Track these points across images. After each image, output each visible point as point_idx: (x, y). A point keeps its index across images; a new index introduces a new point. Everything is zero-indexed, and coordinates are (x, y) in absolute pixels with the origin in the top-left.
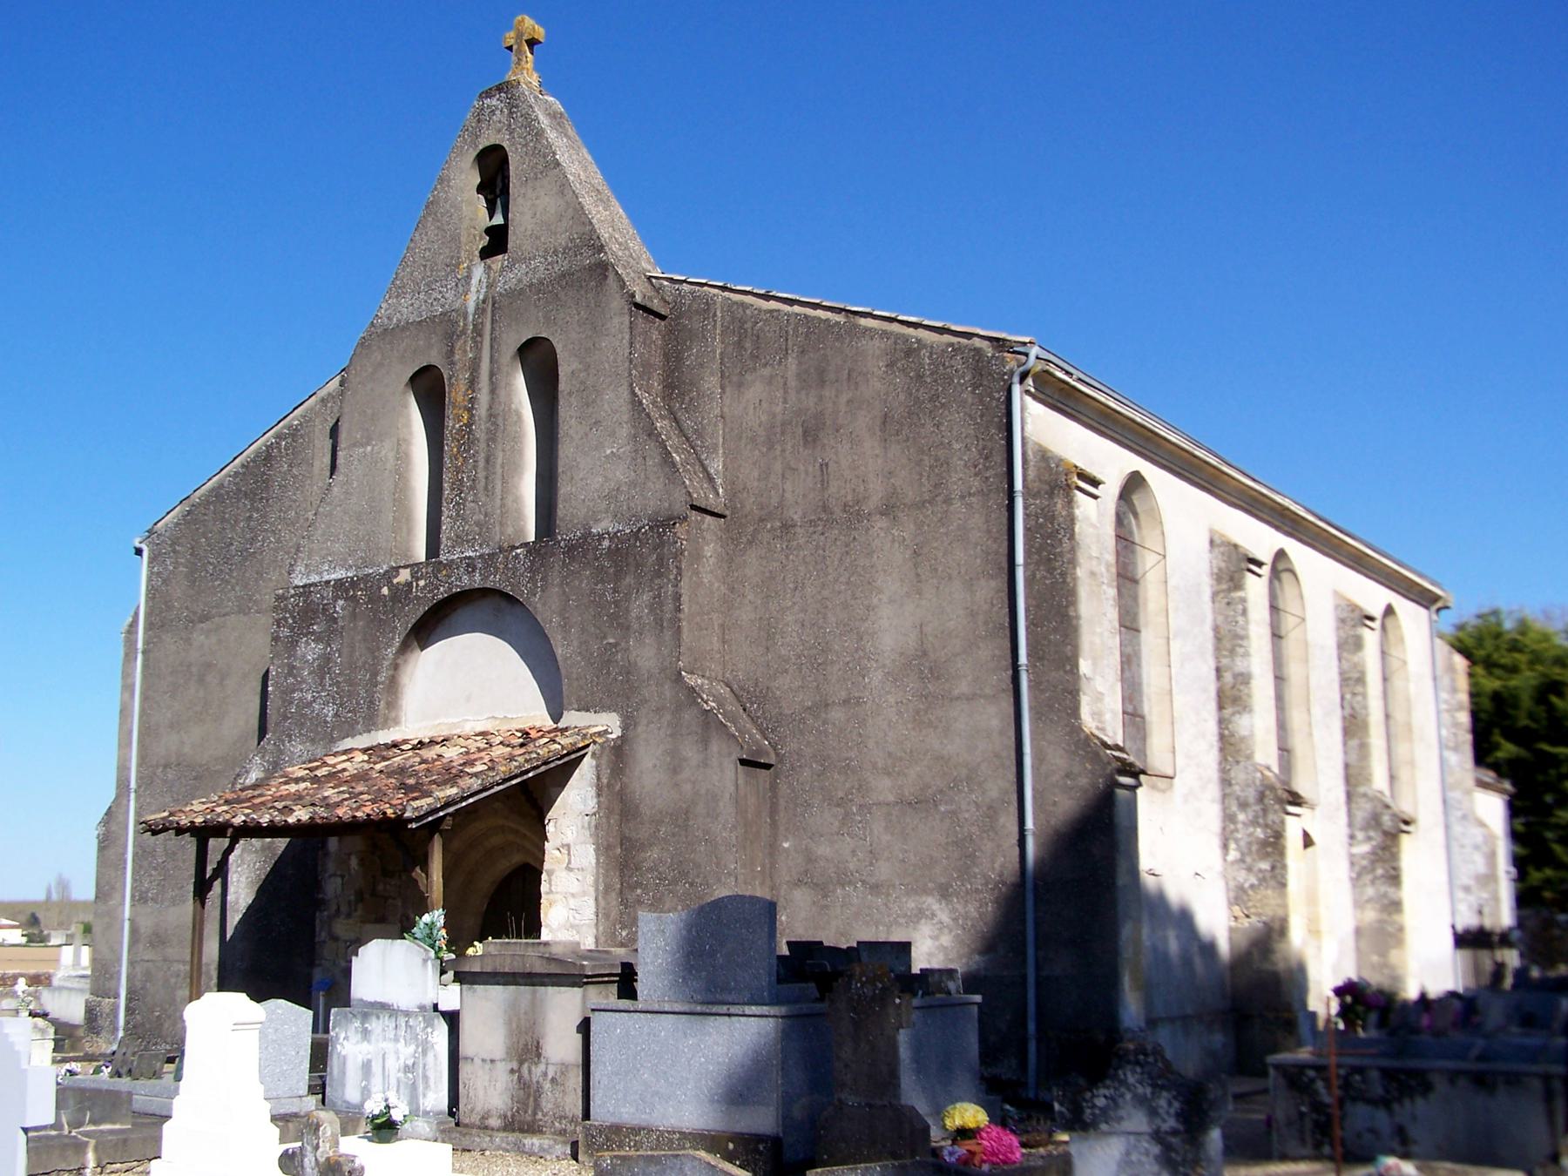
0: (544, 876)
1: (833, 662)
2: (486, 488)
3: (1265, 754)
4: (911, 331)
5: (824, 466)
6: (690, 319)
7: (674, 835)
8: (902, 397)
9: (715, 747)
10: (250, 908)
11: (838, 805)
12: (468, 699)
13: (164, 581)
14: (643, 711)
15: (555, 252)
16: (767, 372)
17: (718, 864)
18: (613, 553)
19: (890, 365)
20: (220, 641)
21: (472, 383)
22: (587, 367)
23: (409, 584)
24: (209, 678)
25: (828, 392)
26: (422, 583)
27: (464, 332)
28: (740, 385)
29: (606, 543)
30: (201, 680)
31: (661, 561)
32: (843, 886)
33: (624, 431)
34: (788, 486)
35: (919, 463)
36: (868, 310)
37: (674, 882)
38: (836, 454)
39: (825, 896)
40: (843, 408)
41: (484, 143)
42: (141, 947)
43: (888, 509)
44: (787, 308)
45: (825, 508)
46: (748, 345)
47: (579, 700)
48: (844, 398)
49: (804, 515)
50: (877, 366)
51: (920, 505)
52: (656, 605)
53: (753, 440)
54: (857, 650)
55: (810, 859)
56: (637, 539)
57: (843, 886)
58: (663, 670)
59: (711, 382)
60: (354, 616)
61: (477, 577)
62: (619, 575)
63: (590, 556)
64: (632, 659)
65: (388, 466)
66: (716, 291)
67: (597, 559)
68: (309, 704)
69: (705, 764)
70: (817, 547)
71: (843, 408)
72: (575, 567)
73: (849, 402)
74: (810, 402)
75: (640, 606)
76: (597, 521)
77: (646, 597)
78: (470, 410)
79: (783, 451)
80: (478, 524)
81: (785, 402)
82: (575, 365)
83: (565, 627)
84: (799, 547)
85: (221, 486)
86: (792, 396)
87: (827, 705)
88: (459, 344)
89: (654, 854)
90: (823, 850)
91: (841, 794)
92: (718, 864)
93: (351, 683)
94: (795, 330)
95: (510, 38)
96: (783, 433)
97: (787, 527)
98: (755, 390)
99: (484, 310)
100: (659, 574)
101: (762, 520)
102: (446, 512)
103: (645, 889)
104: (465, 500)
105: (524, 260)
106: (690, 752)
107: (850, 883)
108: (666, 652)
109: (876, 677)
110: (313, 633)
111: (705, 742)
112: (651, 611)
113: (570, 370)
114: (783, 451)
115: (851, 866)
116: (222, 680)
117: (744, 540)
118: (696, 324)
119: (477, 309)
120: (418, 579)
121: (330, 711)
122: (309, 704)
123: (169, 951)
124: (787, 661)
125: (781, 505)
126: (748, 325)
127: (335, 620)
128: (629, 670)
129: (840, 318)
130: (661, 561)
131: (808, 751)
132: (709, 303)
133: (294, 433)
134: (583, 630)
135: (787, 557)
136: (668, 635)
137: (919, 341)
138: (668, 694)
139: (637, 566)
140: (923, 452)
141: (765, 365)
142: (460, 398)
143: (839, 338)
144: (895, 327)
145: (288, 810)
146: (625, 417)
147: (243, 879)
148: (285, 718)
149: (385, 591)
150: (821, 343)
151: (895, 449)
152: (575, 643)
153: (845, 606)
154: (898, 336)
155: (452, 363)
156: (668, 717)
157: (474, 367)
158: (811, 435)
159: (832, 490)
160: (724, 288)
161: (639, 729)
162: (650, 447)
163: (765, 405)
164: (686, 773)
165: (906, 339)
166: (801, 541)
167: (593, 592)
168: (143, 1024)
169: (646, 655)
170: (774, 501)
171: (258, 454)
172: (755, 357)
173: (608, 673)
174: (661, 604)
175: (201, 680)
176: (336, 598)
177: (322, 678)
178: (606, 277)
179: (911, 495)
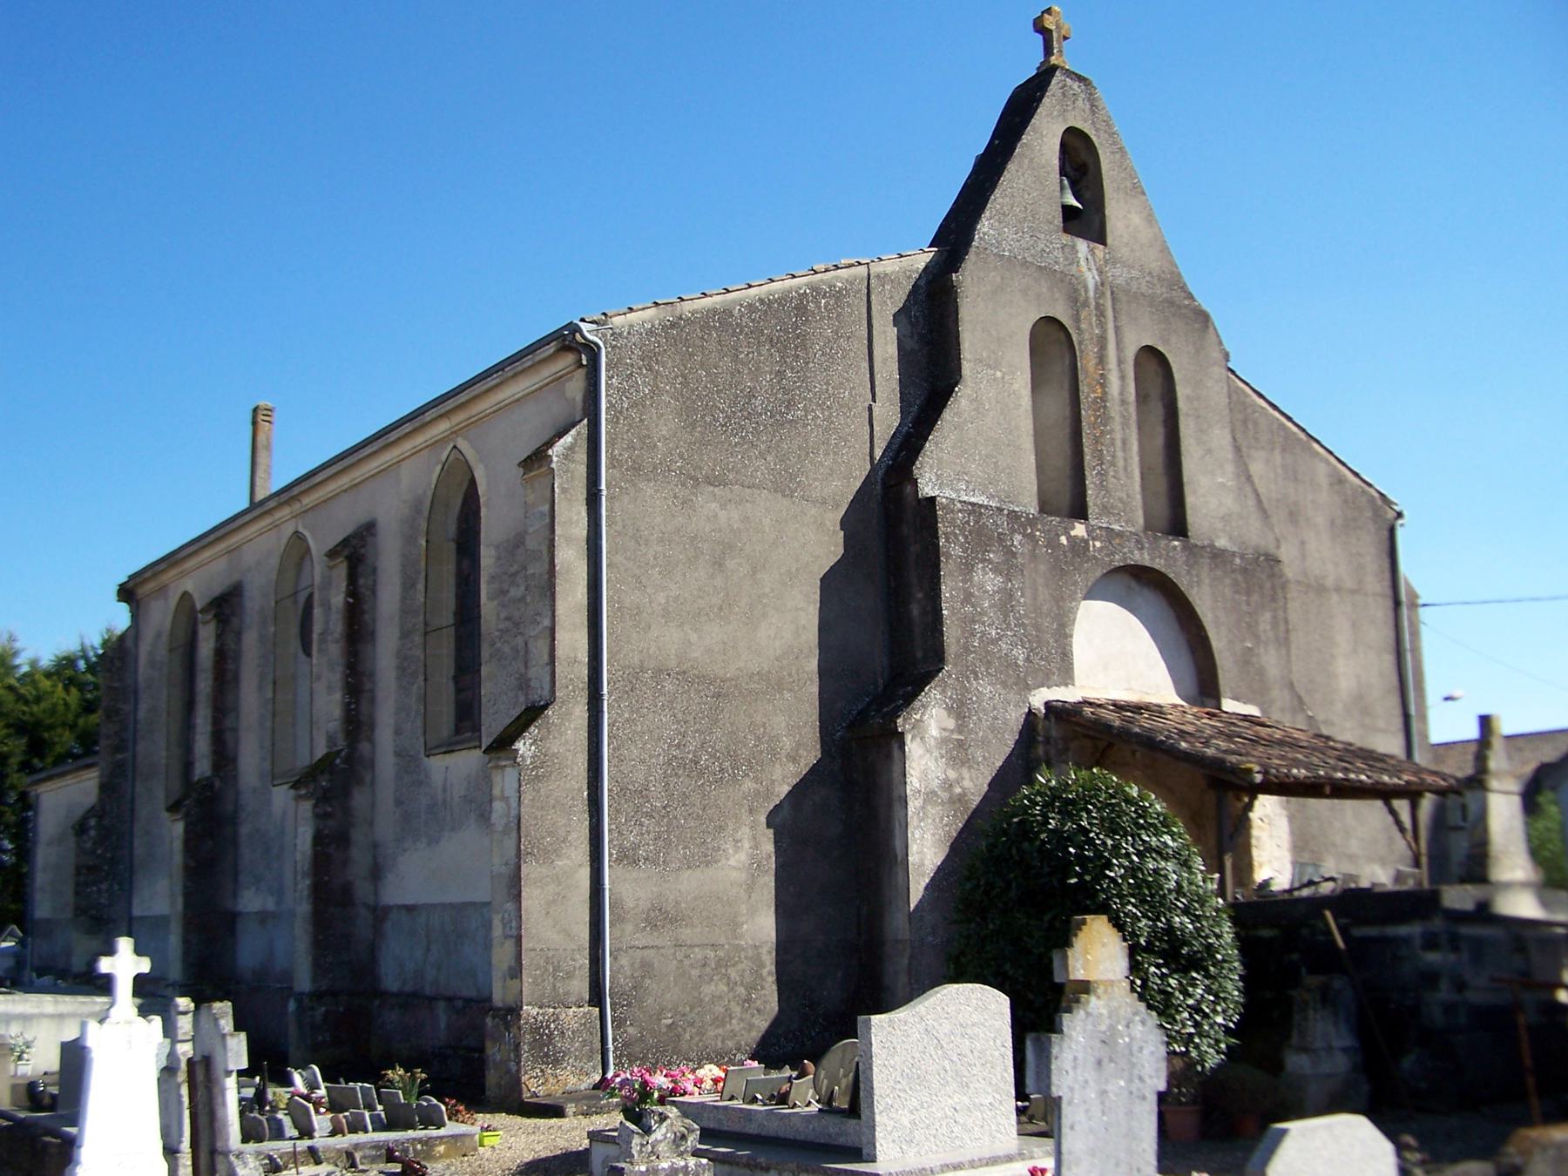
2: (1125, 468)
3: (203, 767)
5: (1303, 543)
10: (940, 869)
13: (634, 405)
20: (745, 519)
21: (1102, 359)
24: (730, 564)
26: (1098, 544)
31: (1273, 588)
42: (629, 928)
43: (1338, 590)
52: (1275, 623)
60: (1033, 556)
62: (1248, 594)
68: (995, 642)
72: (1219, 573)
77: (1268, 616)
78: (1103, 386)
85: (727, 312)
93: (1037, 627)
99: (1103, 294)
109: (1339, 706)
110: (990, 561)
119: (1096, 288)
121: (1020, 654)
122: (995, 642)
123: (686, 934)
127: (1014, 555)
129: (1302, 436)
133: (838, 295)
145: (1289, 767)
147: (928, 836)
149: (1063, 540)
157: (1102, 342)
168: (642, 1039)
171: (784, 298)
175: (719, 564)
177: (1006, 616)
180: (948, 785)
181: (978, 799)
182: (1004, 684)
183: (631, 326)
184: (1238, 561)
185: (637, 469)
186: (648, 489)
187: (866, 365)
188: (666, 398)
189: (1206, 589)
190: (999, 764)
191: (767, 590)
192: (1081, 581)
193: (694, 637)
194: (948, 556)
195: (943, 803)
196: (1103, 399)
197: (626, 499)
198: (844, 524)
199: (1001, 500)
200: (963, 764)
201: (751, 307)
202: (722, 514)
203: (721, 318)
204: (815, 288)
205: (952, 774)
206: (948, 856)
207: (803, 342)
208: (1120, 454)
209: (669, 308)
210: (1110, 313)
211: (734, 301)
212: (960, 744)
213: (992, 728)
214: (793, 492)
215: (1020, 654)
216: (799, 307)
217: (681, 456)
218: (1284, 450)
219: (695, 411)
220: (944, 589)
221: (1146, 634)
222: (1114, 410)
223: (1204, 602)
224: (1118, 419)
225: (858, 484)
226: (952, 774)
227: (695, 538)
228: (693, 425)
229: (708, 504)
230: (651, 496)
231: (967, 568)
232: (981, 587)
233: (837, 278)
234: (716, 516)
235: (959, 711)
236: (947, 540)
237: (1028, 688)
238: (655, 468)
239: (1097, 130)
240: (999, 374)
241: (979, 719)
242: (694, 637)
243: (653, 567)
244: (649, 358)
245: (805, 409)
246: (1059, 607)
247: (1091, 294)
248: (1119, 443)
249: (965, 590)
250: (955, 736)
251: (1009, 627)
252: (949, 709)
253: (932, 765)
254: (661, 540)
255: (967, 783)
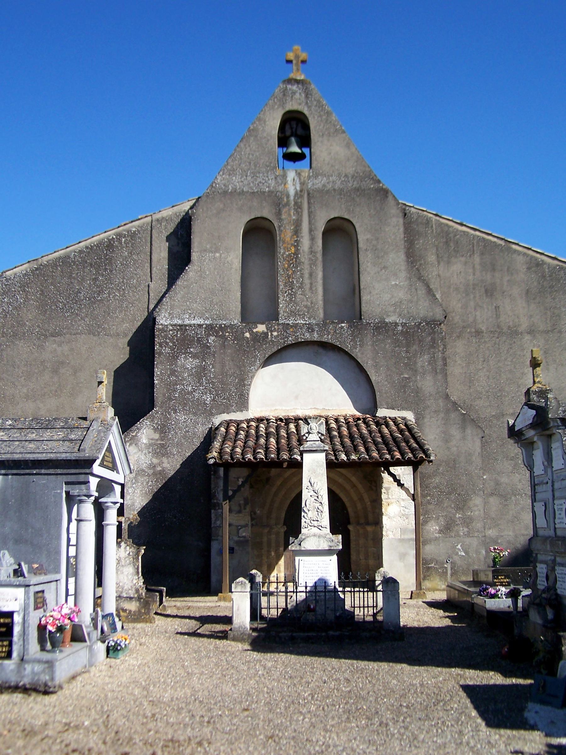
0: (383, 490)
1: (505, 396)
2: (311, 288)
4: (538, 255)
5: (497, 308)
6: (417, 225)
7: (447, 471)
8: (535, 284)
9: (469, 431)
10: (144, 508)
11: (511, 460)
12: (296, 397)
14: (427, 411)
15: (346, 176)
16: (463, 259)
17: (473, 485)
18: (405, 334)
19: (529, 268)
20: (72, 350)
21: (297, 232)
22: (377, 239)
23: (266, 334)
24: (62, 371)
25: (497, 275)
26: (275, 334)
27: (287, 204)
28: (448, 262)
29: (400, 328)
30: (55, 371)
31: (433, 340)
32: (515, 496)
33: (403, 275)
34: (478, 313)
35: (546, 314)
36: (516, 242)
37: (450, 493)
38: (503, 303)
39: (506, 500)
40: (505, 284)
41: (292, 106)
43: (531, 331)
44: (472, 232)
45: (498, 327)
46: (452, 244)
47: (387, 404)
48: (506, 278)
49: (488, 328)
50: (523, 268)
51: (547, 332)
52: (432, 361)
53: (457, 289)
54: (517, 391)
55: (498, 483)
56: (419, 328)
57: (515, 496)
58: (438, 393)
59: (432, 258)
60: (223, 346)
61: (316, 335)
62: (408, 346)
63: (390, 333)
64: (419, 386)
65: (234, 266)
66: (431, 215)
67: (394, 335)
69: (464, 438)
70: (495, 344)
71: (505, 284)
72: (381, 337)
73: (508, 281)
74: (488, 277)
75: (423, 361)
76: (388, 316)
78: (296, 247)
79: (475, 297)
80: (306, 306)
81: (474, 274)
82: (369, 236)
83: (376, 366)
84: (485, 342)
85: (67, 257)
86: (478, 273)
87: (503, 415)
88: (284, 211)
89: (437, 480)
90: (504, 479)
91: (512, 455)
92: (473, 485)
94: (478, 243)
95: (291, 56)
96: (474, 289)
97: (478, 333)
98: (457, 266)
99: (301, 196)
100: (433, 347)
101: (464, 327)
102: (281, 298)
103: (433, 497)
104: (295, 293)
105: (323, 175)
106: (455, 432)
107: (519, 494)
108: (439, 384)
110: (191, 353)
111: (463, 428)
112: (429, 364)
113: (365, 238)
114: (475, 297)
115: (519, 487)
116: (75, 372)
117: (455, 335)
118: (421, 229)
120: (272, 331)
121: (208, 398)
124: (481, 393)
125: (475, 320)
126: (451, 235)
127: (208, 347)
128: (417, 391)
129: (502, 243)
130: (433, 340)
131: (495, 435)
132: (428, 221)
133: (133, 235)
134: (388, 369)
135: (479, 346)
136: (440, 377)
137: (543, 261)
138: (441, 404)
139: (420, 341)
140: (547, 309)
141: (463, 256)
142: (288, 239)
143: (502, 251)
144: (530, 252)
146: (403, 268)
148: (170, 399)
149: (247, 335)
150: (493, 252)
151: (533, 306)
152: (383, 375)
153: (510, 371)
154: (532, 257)
155: (280, 220)
156: (442, 415)
158: (490, 292)
159: (502, 319)
160: (436, 215)
161: (426, 420)
162: (419, 284)
163: (463, 274)
164: (454, 442)
165: (536, 259)
166: (487, 340)
167: (393, 351)
169: (428, 384)
170: (471, 319)
171: (100, 243)
172: (456, 251)
173: (405, 392)
174: (435, 361)
175: (55, 371)
176: (209, 335)
177: (200, 379)
178: (387, 197)
179: (542, 327)
180: (152, 466)
181: (172, 473)
182: (195, 414)
183: (16, 274)
184: (400, 328)
185: (15, 335)
186: (20, 344)
187: (148, 265)
188: (32, 302)
189: (368, 348)
190: (188, 455)
191: (82, 380)
192: (261, 356)
193: (41, 405)
194: (160, 353)
195: (149, 475)
196: (296, 253)
197: (9, 349)
198: (129, 344)
199: (213, 319)
200: (163, 455)
201: (81, 252)
202: (59, 349)
203: (65, 261)
204: (119, 235)
205: (155, 461)
206: (151, 501)
207: (110, 261)
208: (307, 281)
209: (35, 262)
210: (305, 206)
211: (71, 252)
212: (162, 446)
213: (185, 437)
214: (99, 333)
215: (208, 398)
216: (110, 245)
217: (38, 326)
218: (482, 254)
219: (47, 305)
220: (157, 371)
221: (331, 377)
222: (304, 258)
223: (365, 355)
224: (307, 262)
225: (139, 323)
226: (155, 461)
227: (44, 361)
228: (46, 312)
229: (51, 345)
230: (22, 347)
231: (174, 358)
232: (183, 366)
233: (132, 227)
234: (55, 350)
235: (162, 430)
236: (161, 346)
237: (212, 415)
238: (24, 334)
239: (309, 107)
240: (218, 255)
241: (176, 433)
242: (41, 405)
243: (21, 377)
244: (23, 287)
245: (109, 294)
246: (241, 371)
247: (292, 198)
248: (306, 276)
249: (171, 370)
250: (159, 442)
251: (201, 384)
252: (155, 430)
253: (143, 457)
254: (26, 365)
255: (166, 465)
